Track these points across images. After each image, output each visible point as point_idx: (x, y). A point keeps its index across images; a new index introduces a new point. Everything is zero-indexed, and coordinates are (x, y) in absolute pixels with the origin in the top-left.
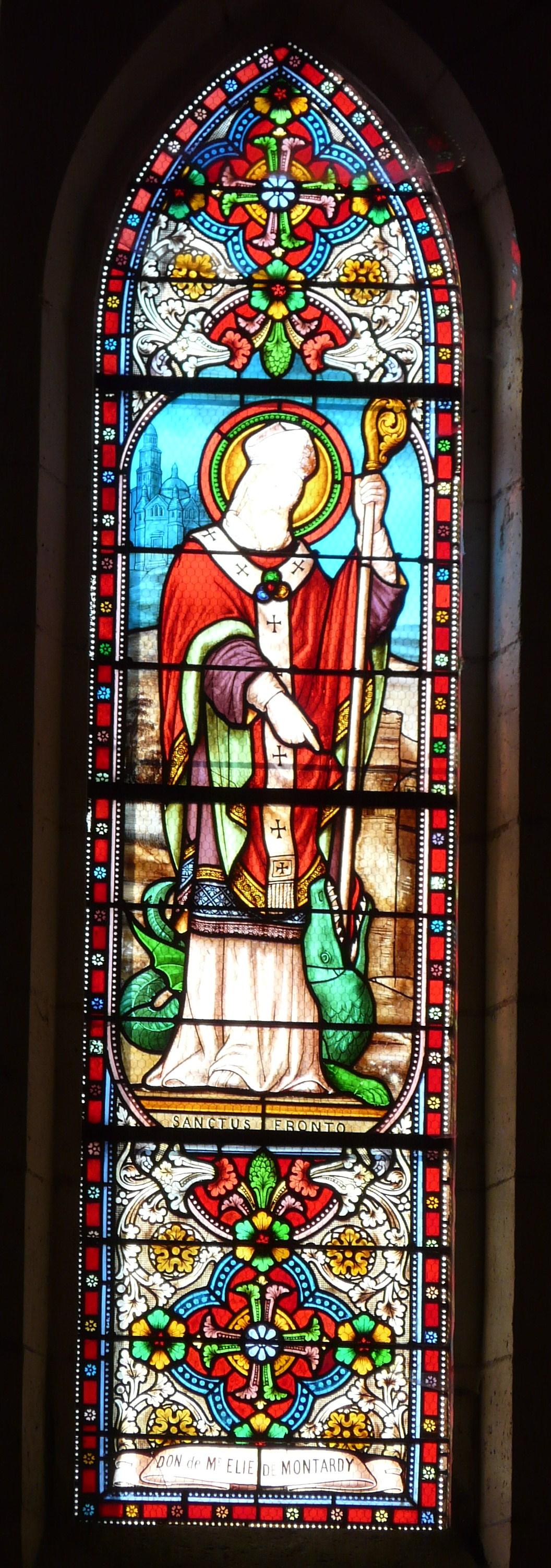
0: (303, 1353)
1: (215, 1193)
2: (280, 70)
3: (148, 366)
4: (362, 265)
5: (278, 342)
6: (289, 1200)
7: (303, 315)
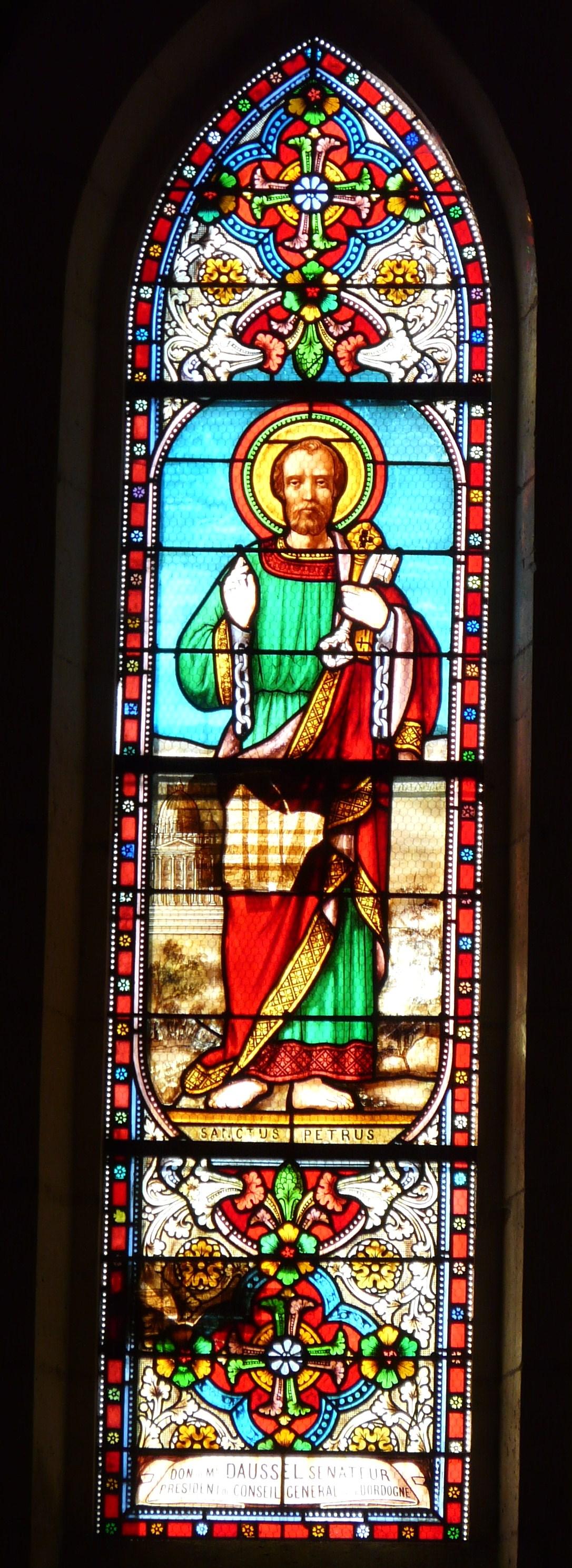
0: (328, 1368)
1: (360, 338)
2: (313, 73)
3: (179, 372)
4: (399, 266)
5: (310, 343)
6: (315, 1213)
7: (337, 316)
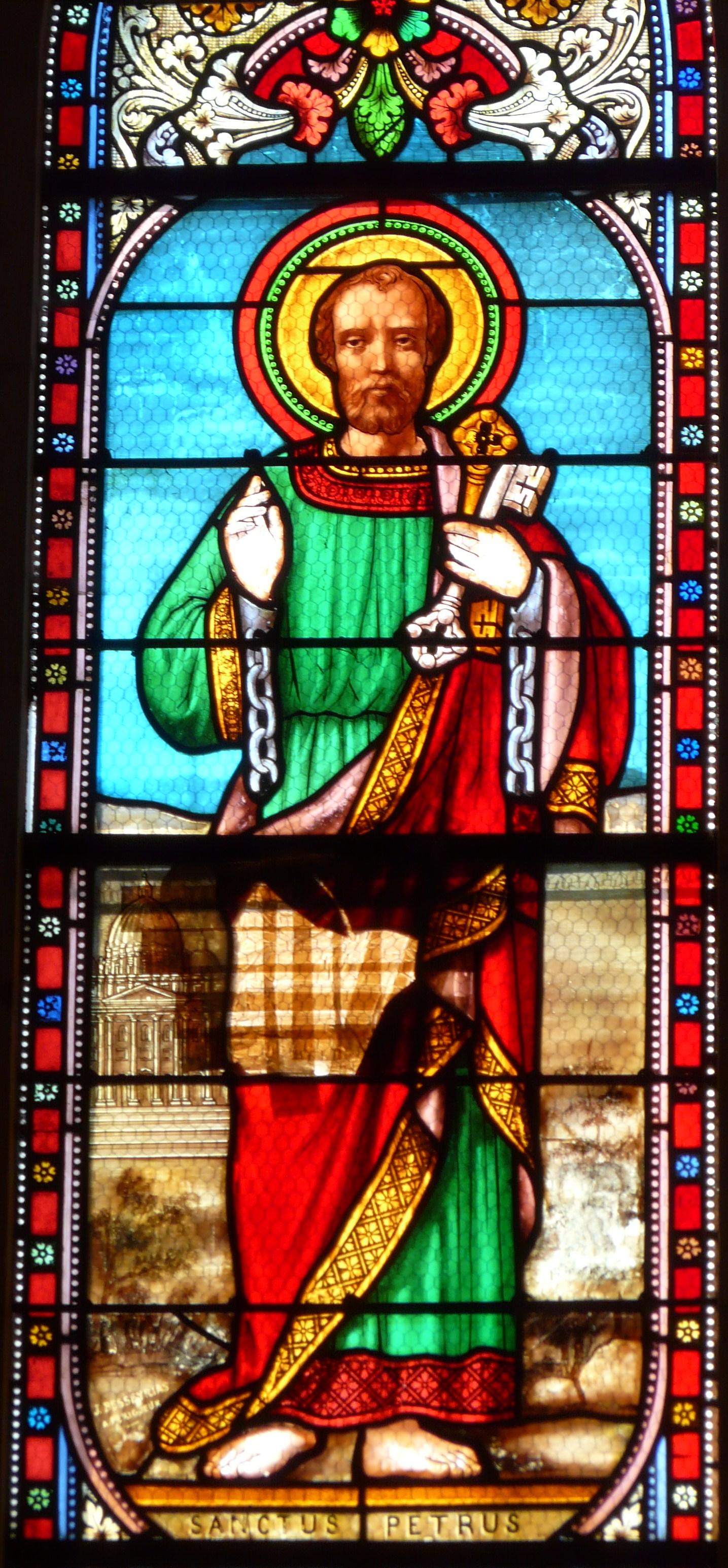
3: (140, 151)
